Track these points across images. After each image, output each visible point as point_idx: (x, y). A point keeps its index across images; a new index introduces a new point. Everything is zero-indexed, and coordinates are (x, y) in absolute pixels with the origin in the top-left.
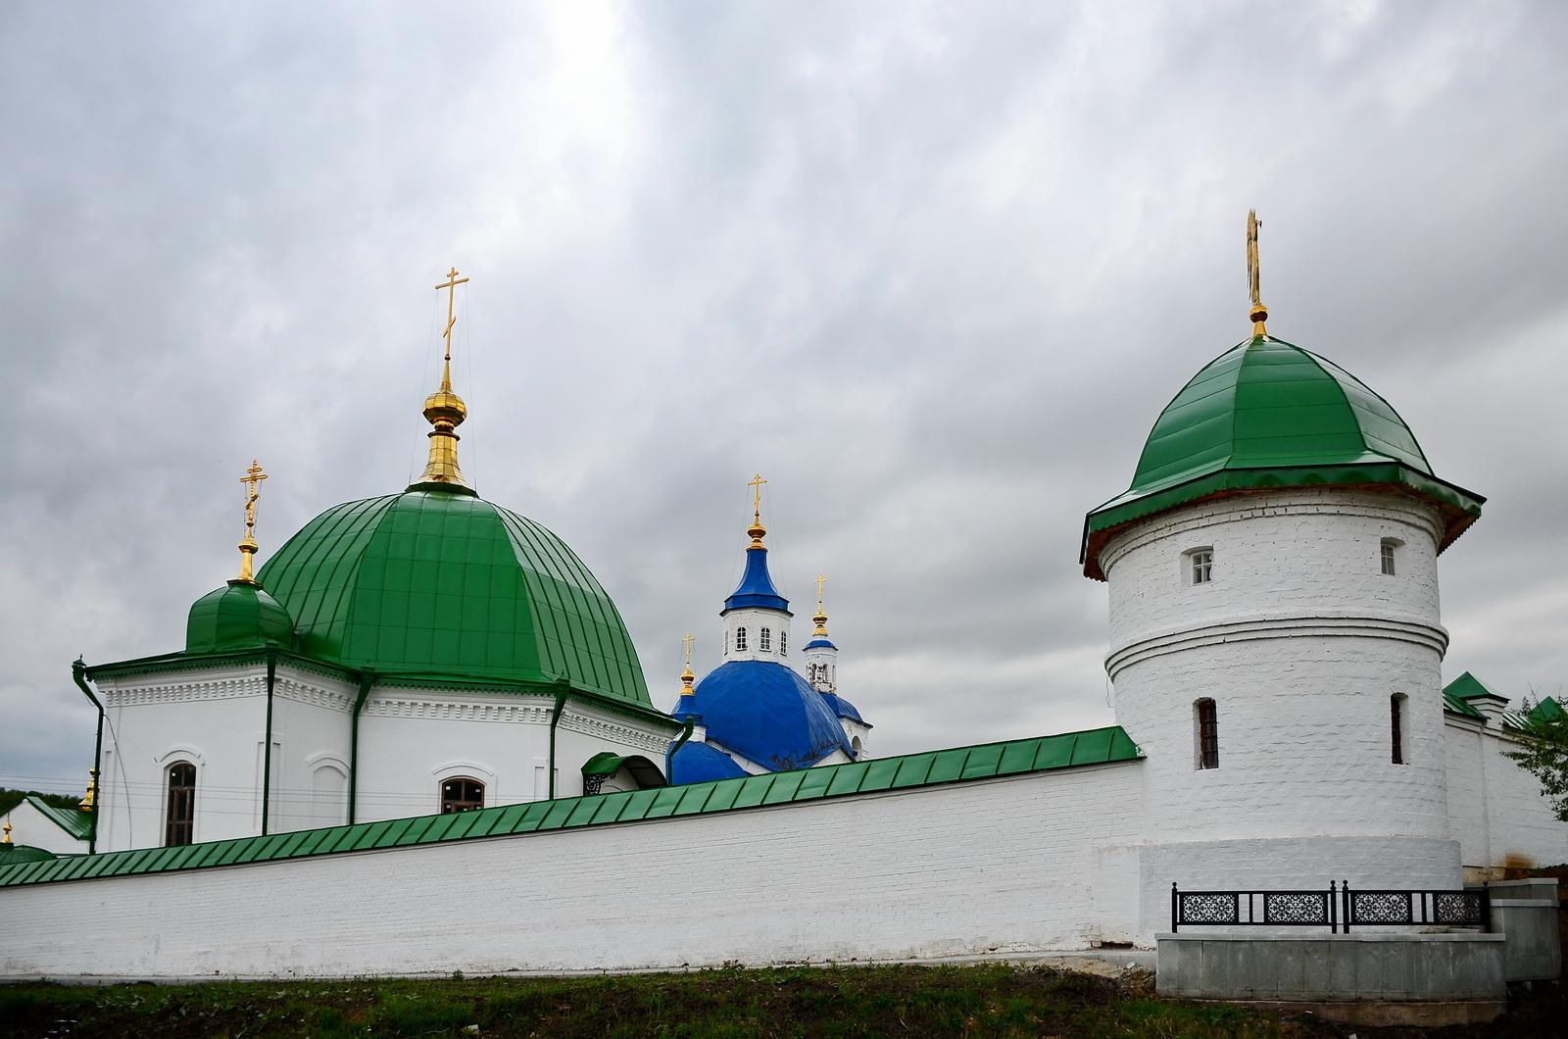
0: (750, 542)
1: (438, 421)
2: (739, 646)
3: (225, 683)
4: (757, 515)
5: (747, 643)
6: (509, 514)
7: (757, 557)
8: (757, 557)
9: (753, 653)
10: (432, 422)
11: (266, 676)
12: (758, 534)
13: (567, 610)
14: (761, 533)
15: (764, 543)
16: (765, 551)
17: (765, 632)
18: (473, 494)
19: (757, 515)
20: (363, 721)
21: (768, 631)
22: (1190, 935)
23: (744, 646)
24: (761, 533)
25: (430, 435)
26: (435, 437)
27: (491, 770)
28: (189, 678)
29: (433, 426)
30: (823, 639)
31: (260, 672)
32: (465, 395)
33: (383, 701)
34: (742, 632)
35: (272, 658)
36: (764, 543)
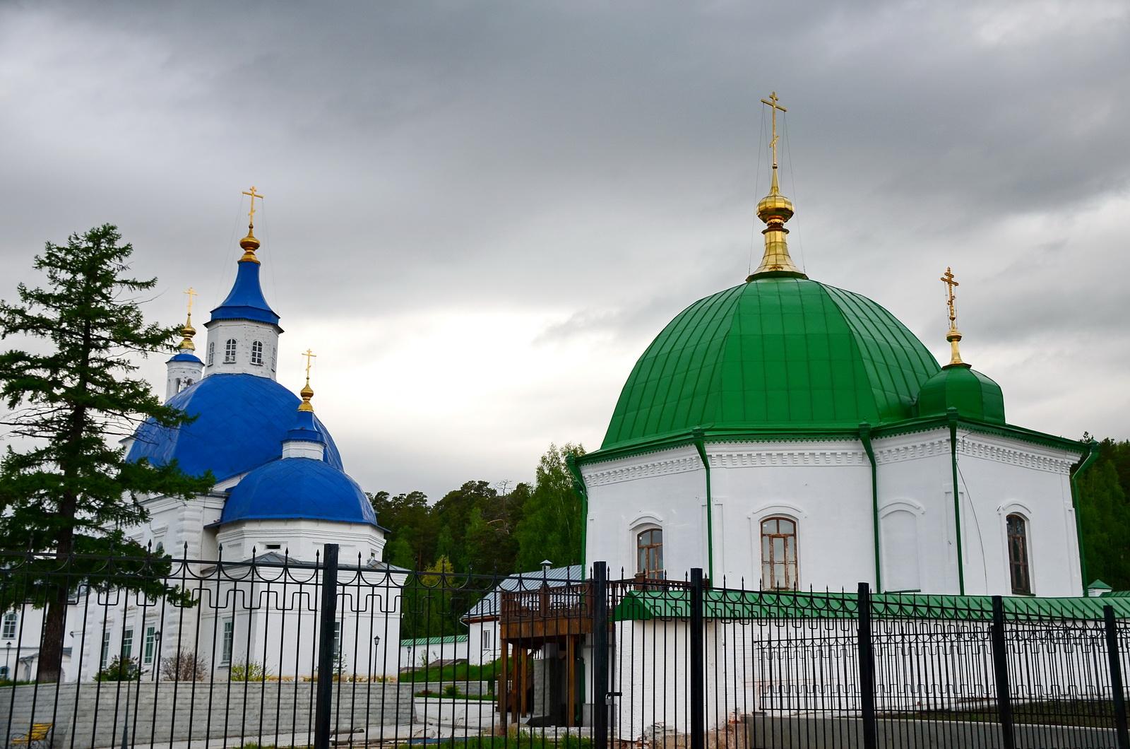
0: (241, 253)
1: (770, 220)
2: (254, 360)
3: (672, 462)
4: (251, 227)
5: (263, 359)
6: (836, 291)
7: (249, 270)
8: (249, 270)
9: (243, 365)
10: (765, 221)
11: (950, 437)
12: (250, 245)
13: (889, 363)
14: (256, 246)
15: (258, 255)
16: (258, 264)
18: (803, 276)
19: (251, 227)
20: (879, 469)
21: (260, 344)
22: (256, 626)
23: (259, 361)
24: (256, 246)
25: (764, 232)
26: (768, 234)
27: (918, 504)
28: (1028, 449)
29: (766, 224)
31: (946, 434)
32: (258, 236)
33: (885, 450)
34: (231, 344)
35: (952, 423)
36: (258, 255)
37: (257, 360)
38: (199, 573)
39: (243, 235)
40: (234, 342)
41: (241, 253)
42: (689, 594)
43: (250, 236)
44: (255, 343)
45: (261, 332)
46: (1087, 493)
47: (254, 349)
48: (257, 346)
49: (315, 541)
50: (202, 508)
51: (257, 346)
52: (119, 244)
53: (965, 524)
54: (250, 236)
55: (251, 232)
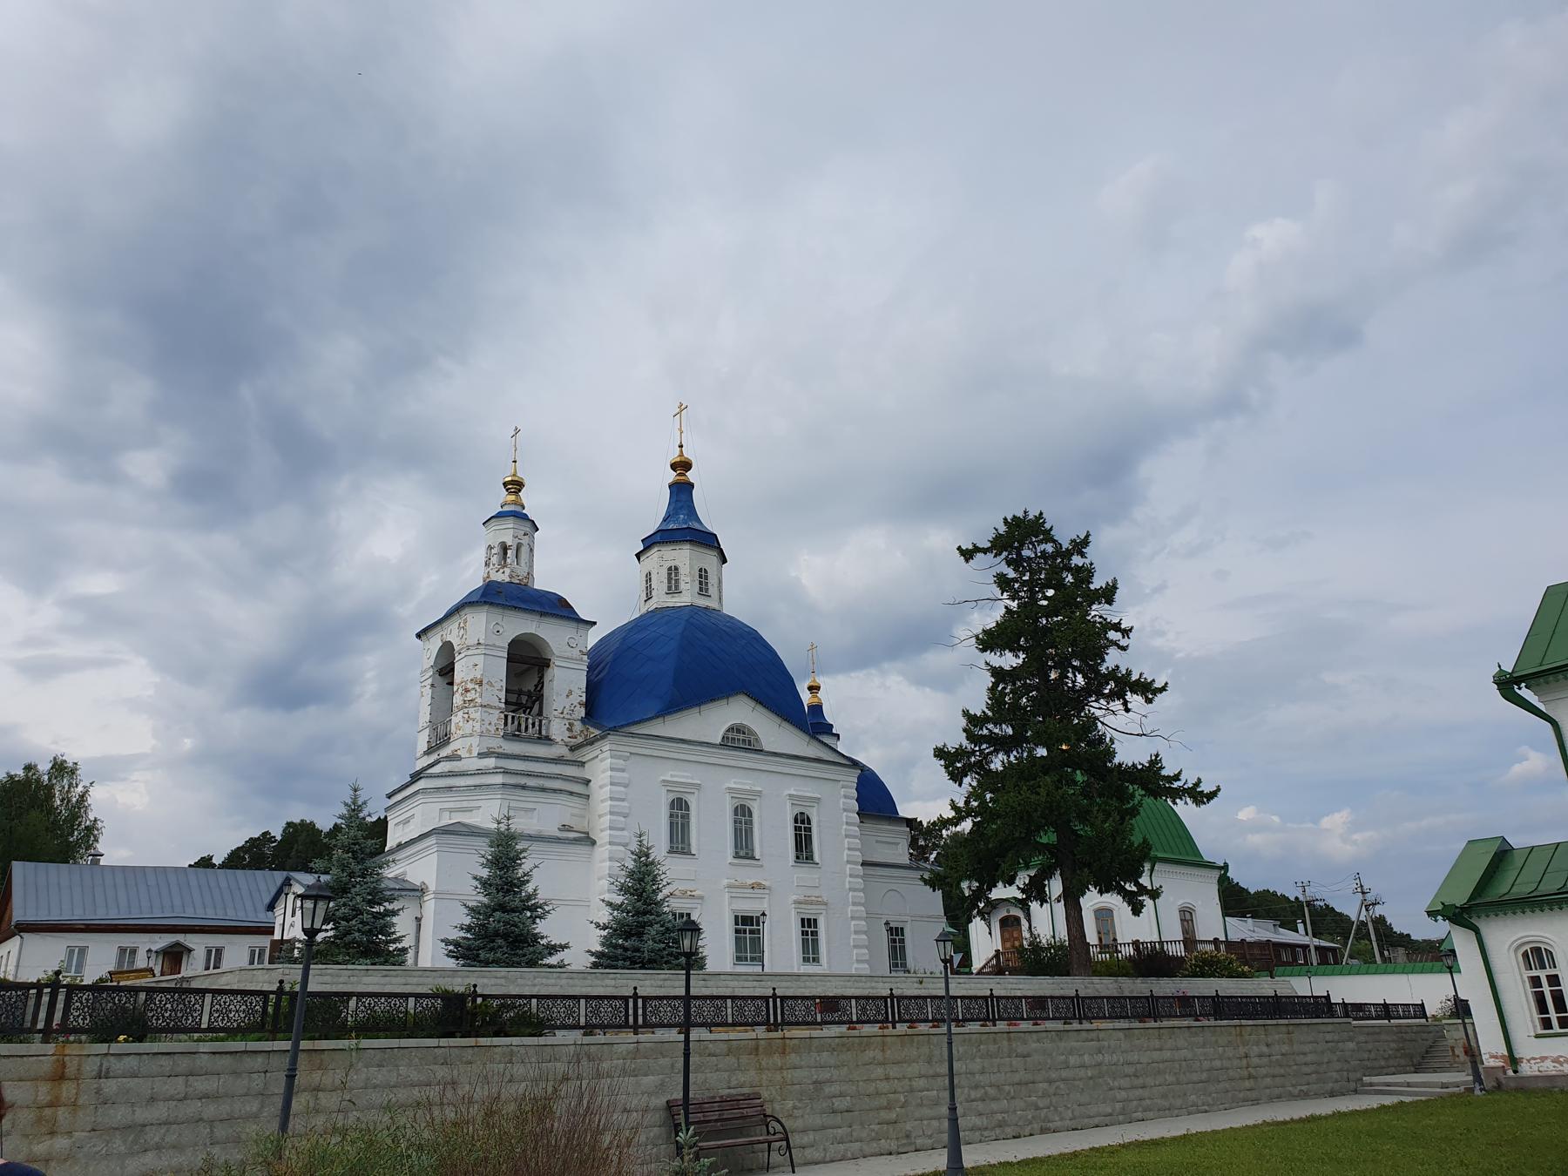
0: (671, 476)
4: (681, 446)
7: (681, 491)
8: (681, 491)
9: (687, 596)
17: (673, 572)
30: (518, 509)
37: (703, 590)
38: (1060, 904)
39: (674, 456)
40: (676, 569)
41: (671, 476)
42: (546, 1031)
43: (681, 454)
44: (700, 570)
45: (709, 560)
46: (1335, 1059)
47: (700, 576)
48: (703, 574)
49: (879, 839)
50: (628, 754)
51: (703, 574)
52: (1098, 583)
53: (1151, 926)
54: (681, 454)
55: (681, 452)
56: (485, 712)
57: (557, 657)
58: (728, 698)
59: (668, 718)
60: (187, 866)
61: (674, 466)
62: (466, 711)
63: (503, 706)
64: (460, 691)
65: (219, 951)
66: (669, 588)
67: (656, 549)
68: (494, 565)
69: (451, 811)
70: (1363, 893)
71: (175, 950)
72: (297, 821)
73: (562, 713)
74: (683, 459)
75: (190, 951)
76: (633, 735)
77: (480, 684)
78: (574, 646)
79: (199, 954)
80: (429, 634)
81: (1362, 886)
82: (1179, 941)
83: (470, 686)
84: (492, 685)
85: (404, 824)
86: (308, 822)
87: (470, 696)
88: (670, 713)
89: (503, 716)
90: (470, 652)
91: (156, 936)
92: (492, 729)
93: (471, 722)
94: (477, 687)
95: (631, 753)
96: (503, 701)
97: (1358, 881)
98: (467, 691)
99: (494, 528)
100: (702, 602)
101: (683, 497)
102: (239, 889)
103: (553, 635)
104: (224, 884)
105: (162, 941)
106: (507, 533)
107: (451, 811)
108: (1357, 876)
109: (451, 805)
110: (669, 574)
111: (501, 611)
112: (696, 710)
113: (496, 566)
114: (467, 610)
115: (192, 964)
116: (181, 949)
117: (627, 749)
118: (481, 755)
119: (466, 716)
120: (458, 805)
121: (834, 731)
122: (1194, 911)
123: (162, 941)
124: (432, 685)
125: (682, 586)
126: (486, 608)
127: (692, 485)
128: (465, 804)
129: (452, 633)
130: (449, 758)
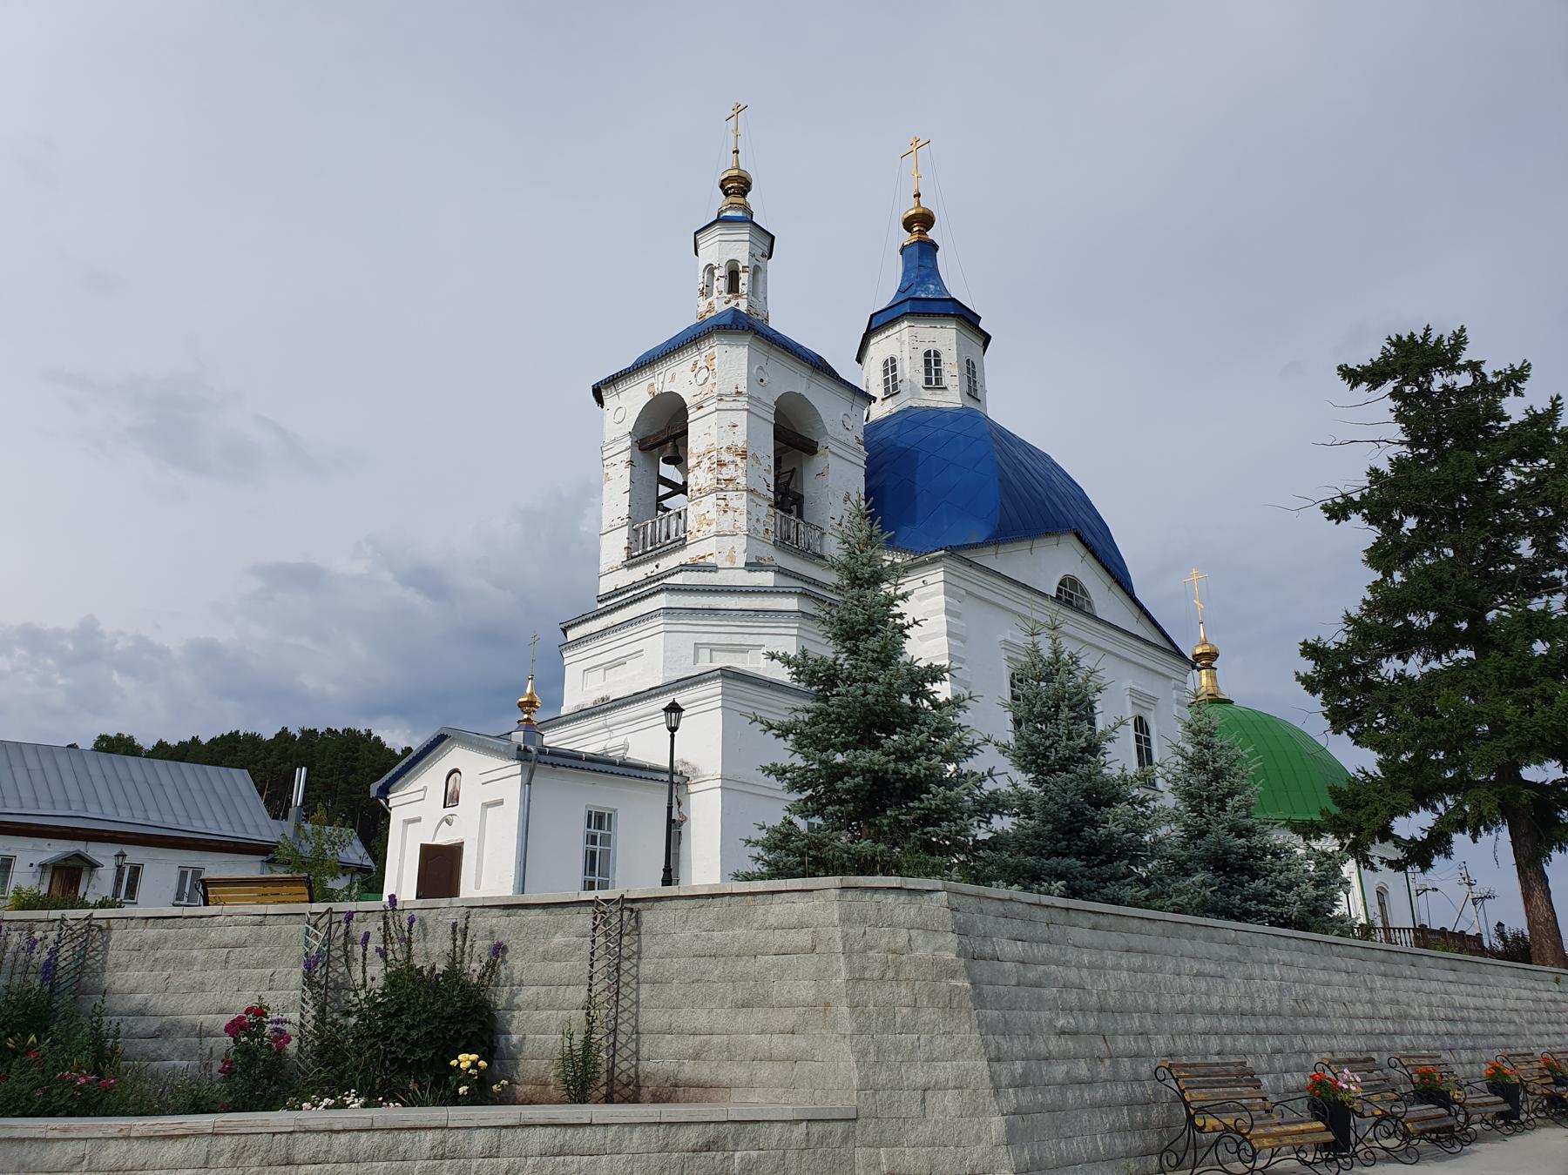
0: (906, 238)
7: (922, 254)
8: (922, 254)
40: (937, 354)
56: (752, 500)
57: (832, 438)
58: (1059, 536)
59: (1002, 549)
60: (87, 743)
61: (908, 224)
62: (721, 495)
63: (772, 496)
64: (706, 464)
65: (136, 870)
66: (928, 381)
67: (906, 324)
68: (720, 292)
69: (713, 648)
70: (1470, 884)
71: (70, 863)
72: (113, 734)
73: (840, 525)
74: (921, 210)
75: (93, 866)
76: (972, 564)
77: (744, 455)
78: (850, 428)
79: (107, 873)
80: (621, 387)
81: (1468, 877)
82: (1409, 929)
83: (726, 457)
84: (758, 461)
85: (606, 669)
86: (126, 736)
87: (727, 473)
88: (1005, 542)
89: (772, 513)
90: (722, 405)
91: (42, 843)
92: (762, 529)
93: (730, 513)
94: (738, 459)
95: (967, 592)
96: (772, 489)
97: (1463, 871)
98: (721, 464)
99: (718, 238)
100: (971, 404)
101: (927, 262)
102: (162, 785)
103: (829, 408)
104: (138, 777)
105: (55, 850)
106: (734, 247)
107: (713, 648)
108: (1463, 865)
109: (714, 639)
110: (927, 362)
111: (766, 348)
112: (1026, 545)
113: (725, 294)
114: (714, 341)
115: (94, 887)
116: (79, 863)
117: (963, 584)
118: (752, 566)
119: (722, 503)
120: (725, 639)
121: (399, 752)
122: (1387, 892)
123: (55, 850)
124: (631, 463)
125: (947, 380)
126: (749, 338)
127: (936, 248)
128: (736, 639)
129: (678, 378)
130: (693, 567)
